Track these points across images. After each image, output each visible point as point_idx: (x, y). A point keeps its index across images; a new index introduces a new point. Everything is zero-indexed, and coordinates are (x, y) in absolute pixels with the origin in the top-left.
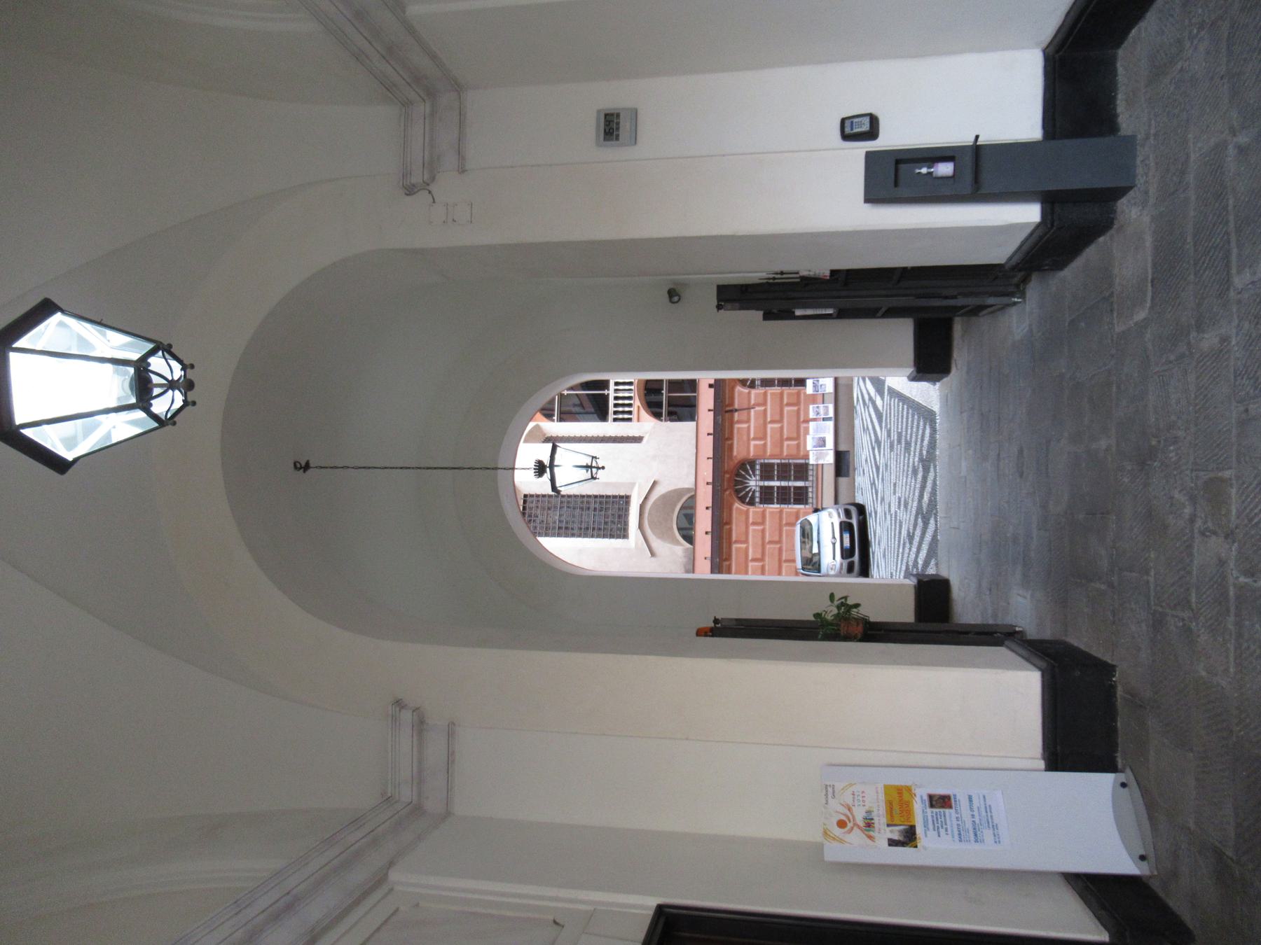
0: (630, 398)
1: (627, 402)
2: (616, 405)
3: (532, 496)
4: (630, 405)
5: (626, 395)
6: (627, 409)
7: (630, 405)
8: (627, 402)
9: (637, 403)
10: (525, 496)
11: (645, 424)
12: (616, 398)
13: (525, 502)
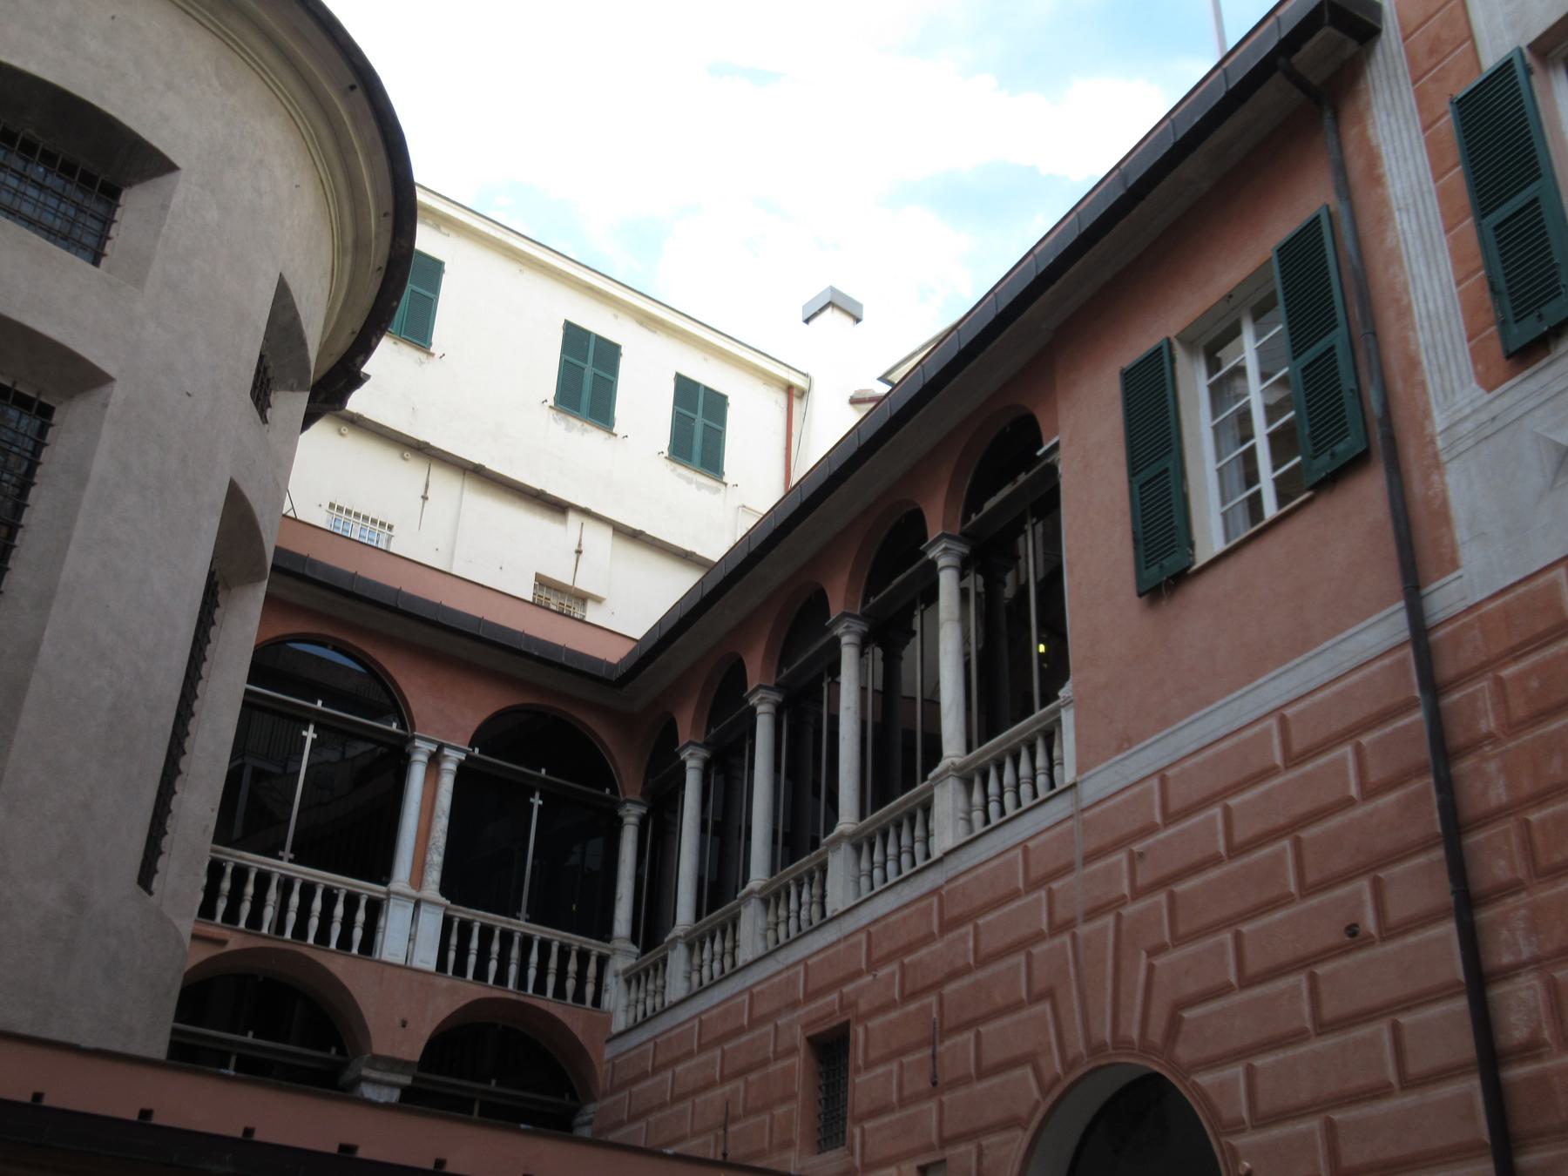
0: (255, 920)
1: (246, 908)
2: (240, 874)
3: (42, 431)
4: (231, 916)
5: (269, 913)
6: (222, 905)
7: (231, 916)
8: (246, 908)
9: (236, 941)
10: (46, 412)
11: (174, 927)
12: (263, 879)
13: (23, 402)
